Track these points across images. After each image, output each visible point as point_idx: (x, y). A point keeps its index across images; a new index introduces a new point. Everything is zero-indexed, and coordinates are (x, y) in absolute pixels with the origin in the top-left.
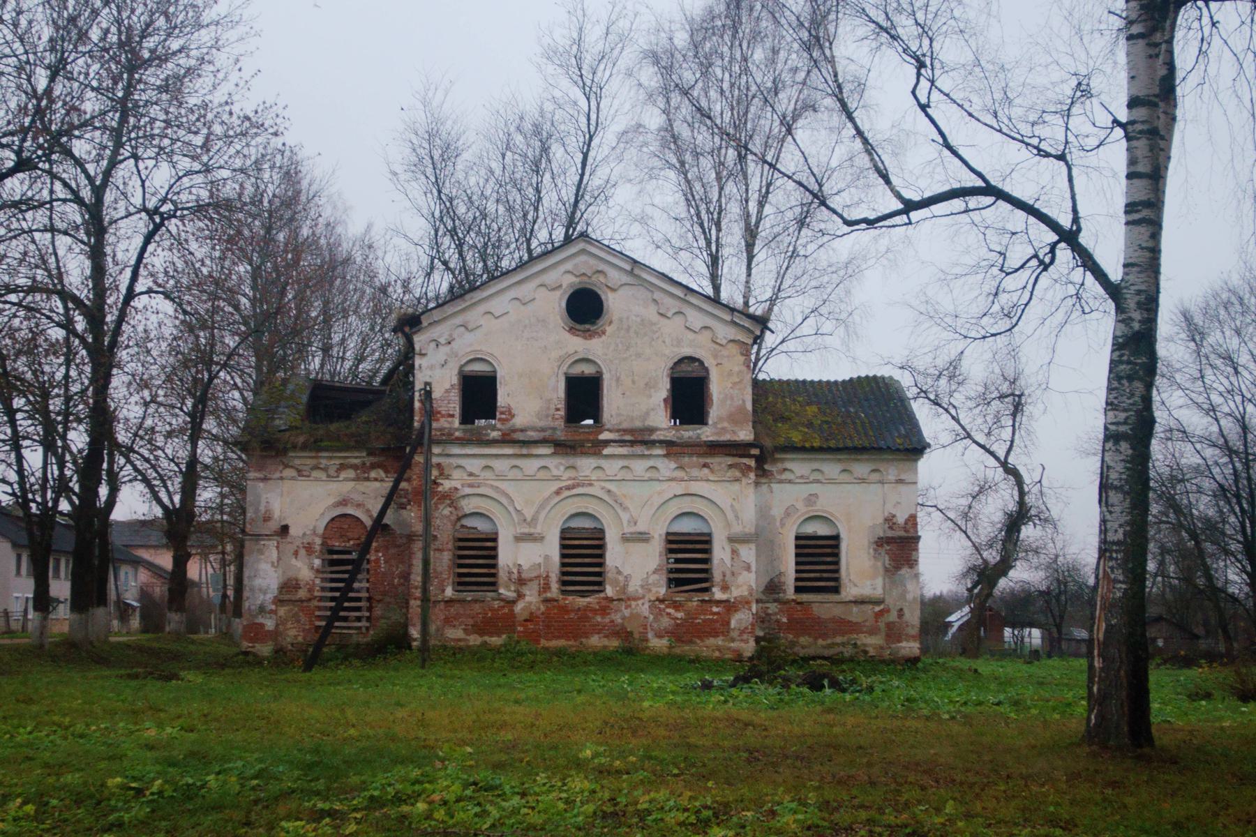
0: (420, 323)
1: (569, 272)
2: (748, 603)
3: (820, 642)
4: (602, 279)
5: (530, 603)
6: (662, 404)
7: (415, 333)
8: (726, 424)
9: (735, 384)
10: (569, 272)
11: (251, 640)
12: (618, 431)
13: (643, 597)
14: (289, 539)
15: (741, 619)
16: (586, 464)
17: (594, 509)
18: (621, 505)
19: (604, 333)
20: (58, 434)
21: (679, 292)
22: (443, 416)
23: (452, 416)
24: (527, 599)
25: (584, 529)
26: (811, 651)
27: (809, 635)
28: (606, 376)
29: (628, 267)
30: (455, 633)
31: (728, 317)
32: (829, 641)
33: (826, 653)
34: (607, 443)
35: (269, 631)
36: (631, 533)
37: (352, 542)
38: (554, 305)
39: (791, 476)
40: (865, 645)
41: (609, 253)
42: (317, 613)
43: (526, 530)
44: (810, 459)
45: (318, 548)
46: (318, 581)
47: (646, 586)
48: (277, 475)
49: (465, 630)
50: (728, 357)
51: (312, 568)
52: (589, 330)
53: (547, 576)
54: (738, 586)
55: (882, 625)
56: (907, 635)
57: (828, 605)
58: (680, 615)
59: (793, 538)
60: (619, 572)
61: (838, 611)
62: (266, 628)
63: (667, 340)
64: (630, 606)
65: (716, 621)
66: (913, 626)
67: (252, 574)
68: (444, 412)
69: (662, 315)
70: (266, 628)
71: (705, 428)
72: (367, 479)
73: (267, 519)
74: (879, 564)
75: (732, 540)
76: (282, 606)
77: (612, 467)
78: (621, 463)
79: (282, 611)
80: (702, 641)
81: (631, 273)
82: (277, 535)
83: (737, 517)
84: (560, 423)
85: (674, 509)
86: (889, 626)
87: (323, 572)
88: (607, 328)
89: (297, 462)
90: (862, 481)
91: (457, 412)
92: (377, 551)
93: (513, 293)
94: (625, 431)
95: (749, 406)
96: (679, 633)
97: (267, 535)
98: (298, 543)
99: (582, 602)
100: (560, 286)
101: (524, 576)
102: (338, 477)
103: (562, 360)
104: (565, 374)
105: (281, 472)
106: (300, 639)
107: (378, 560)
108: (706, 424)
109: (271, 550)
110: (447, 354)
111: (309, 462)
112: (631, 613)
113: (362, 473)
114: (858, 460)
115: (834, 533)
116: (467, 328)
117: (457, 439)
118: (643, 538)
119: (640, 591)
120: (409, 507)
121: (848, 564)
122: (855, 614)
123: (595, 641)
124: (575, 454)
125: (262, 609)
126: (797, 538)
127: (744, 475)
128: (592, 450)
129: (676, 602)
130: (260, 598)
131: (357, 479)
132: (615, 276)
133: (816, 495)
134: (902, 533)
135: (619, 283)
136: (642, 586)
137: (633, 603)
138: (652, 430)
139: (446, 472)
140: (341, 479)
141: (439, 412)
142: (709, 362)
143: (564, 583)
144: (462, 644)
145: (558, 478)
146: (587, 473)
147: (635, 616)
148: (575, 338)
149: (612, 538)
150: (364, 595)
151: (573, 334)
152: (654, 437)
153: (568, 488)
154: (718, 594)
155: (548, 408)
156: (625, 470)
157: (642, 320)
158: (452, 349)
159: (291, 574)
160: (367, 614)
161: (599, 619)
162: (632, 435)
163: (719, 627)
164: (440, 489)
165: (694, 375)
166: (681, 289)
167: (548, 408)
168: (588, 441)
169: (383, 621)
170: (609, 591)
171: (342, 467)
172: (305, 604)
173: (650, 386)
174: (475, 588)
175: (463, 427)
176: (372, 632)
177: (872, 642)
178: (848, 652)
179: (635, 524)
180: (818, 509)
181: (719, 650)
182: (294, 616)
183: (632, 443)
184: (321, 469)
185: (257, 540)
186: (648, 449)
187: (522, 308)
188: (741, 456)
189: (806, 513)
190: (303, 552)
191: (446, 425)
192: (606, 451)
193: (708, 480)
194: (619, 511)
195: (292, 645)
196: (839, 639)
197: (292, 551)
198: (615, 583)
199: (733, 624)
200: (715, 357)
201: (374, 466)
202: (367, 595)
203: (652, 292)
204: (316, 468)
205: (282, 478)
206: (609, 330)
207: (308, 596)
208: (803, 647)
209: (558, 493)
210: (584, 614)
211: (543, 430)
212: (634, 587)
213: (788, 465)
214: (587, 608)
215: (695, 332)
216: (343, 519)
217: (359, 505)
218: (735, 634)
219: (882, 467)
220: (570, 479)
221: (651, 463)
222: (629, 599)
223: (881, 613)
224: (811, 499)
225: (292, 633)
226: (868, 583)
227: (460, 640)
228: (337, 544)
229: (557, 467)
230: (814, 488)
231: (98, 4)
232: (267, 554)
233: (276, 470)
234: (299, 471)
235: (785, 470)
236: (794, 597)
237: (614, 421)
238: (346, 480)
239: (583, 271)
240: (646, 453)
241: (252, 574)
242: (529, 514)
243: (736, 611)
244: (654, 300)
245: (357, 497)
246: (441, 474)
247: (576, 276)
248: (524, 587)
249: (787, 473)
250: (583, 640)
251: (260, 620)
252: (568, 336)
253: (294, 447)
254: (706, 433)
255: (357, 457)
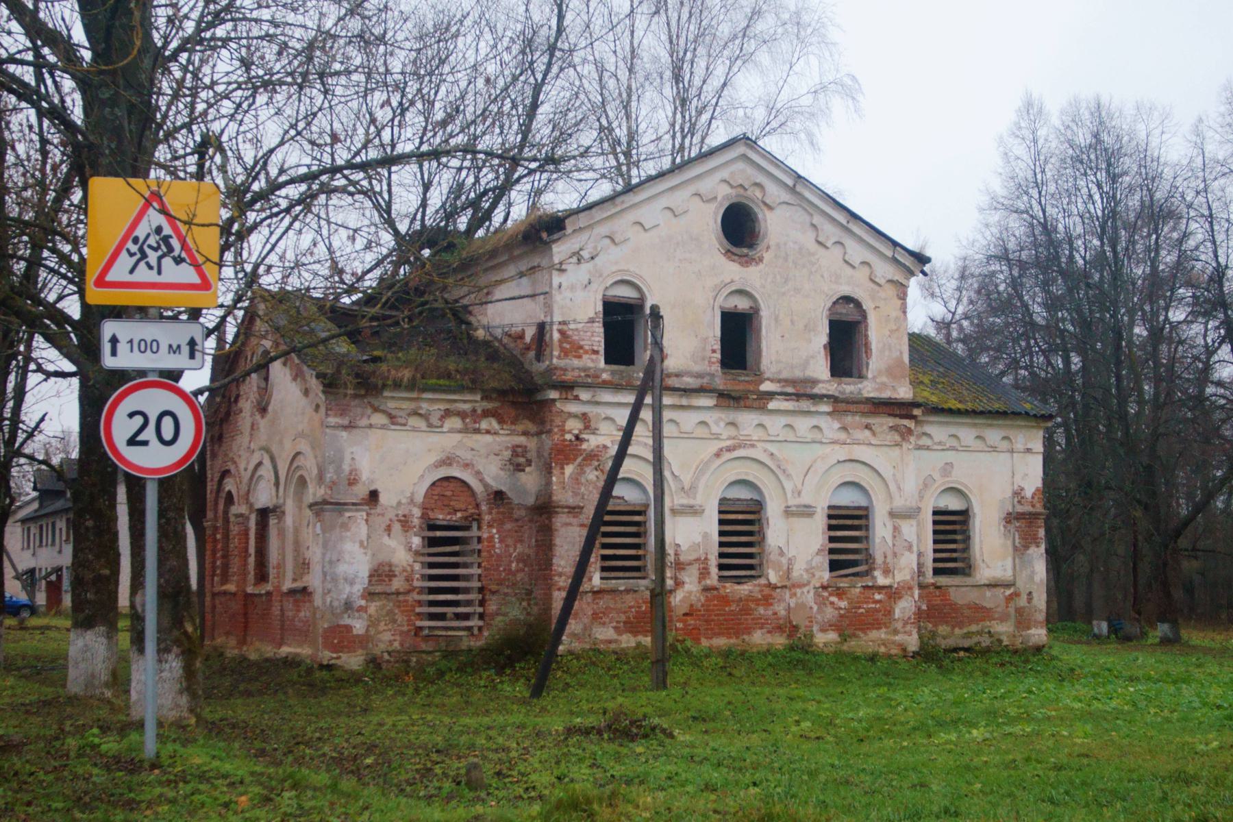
0: (563, 228)
1: (725, 181)
2: (910, 588)
3: (957, 631)
4: (758, 194)
5: (690, 593)
7: (555, 241)
8: (884, 379)
9: (891, 331)
10: (725, 181)
11: (336, 649)
12: (779, 381)
13: (808, 583)
14: (379, 510)
15: (905, 607)
16: (748, 420)
17: (756, 477)
18: (784, 471)
19: (761, 260)
20: (221, 341)
21: (841, 217)
22: (586, 352)
24: (687, 587)
25: (739, 500)
26: (951, 642)
27: (947, 623)
28: (765, 313)
29: (790, 182)
30: (604, 633)
31: (889, 253)
32: (965, 630)
33: (967, 643)
34: (771, 395)
35: (358, 636)
36: (798, 506)
37: (459, 515)
38: (709, 221)
40: (1000, 634)
41: (772, 162)
42: (418, 610)
43: (685, 501)
44: (947, 423)
46: (417, 567)
47: (810, 570)
48: (364, 422)
49: (616, 628)
50: (885, 299)
51: (410, 549)
52: (746, 256)
53: (706, 559)
54: (901, 570)
55: (1012, 610)
56: (1035, 621)
57: (964, 589)
58: (843, 604)
59: (931, 512)
60: (782, 553)
61: (972, 596)
62: (355, 632)
63: (826, 275)
64: (795, 594)
65: (878, 611)
66: (1041, 611)
67: (334, 558)
68: (587, 348)
70: (355, 632)
71: (865, 383)
72: (478, 431)
73: (353, 482)
74: (1009, 543)
75: (892, 515)
76: (373, 601)
77: (775, 424)
78: (784, 420)
79: (373, 608)
80: (866, 634)
81: (792, 190)
82: (366, 504)
85: (839, 476)
86: (1019, 611)
87: (423, 555)
89: (391, 405)
90: (994, 449)
91: (602, 349)
92: (490, 526)
93: (664, 201)
94: (787, 382)
95: (906, 358)
96: (850, 624)
97: (354, 504)
98: (391, 514)
99: (745, 589)
100: (716, 198)
101: (682, 558)
102: (442, 426)
103: (718, 290)
104: (721, 307)
105: (369, 417)
106: (396, 645)
107: (491, 538)
108: (861, 377)
109: (359, 525)
110: (590, 272)
111: (406, 405)
112: (797, 604)
113: (471, 427)
114: (990, 425)
115: (963, 508)
116: (613, 240)
117: (604, 382)
118: (806, 512)
119: (805, 576)
120: (528, 469)
121: (981, 541)
122: (991, 599)
123: (759, 638)
124: (737, 408)
125: (348, 606)
126: (935, 513)
127: (904, 439)
128: (756, 404)
129: (838, 588)
130: (346, 591)
131: (465, 430)
132: (774, 192)
133: (951, 465)
134: (1030, 509)
135: (778, 201)
136: (807, 570)
137: (798, 591)
138: (815, 382)
139: (593, 425)
140: (445, 429)
142: (867, 305)
143: (721, 567)
144: (613, 646)
147: (801, 606)
148: (732, 263)
149: (773, 510)
150: (476, 584)
151: (729, 258)
152: (816, 391)
153: (729, 449)
154: (882, 580)
156: (788, 429)
157: (801, 249)
158: (596, 265)
159: (382, 557)
160: (480, 610)
161: (761, 610)
162: (794, 387)
163: (879, 618)
164: (584, 446)
165: (850, 319)
166: (845, 214)
167: (704, 349)
168: (753, 392)
169: (500, 618)
170: (773, 577)
171: (448, 413)
172: (401, 598)
173: (809, 328)
174: (621, 574)
175: (608, 367)
176: (486, 634)
177: (1003, 629)
178: (986, 641)
179: (799, 493)
180: (952, 481)
181: (884, 644)
182: (390, 612)
183: (798, 396)
184: (420, 415)
185: (341, 513)
186: (814, 404)
187: (674, 221)
188: (902, 417)
189: (944, 483)
190: (397, 527)
191: (590, 364)
192: (772, 405)
193: (871, 444)
194: (782, 478)
195: (389, 653)
196: (974, 628)
197: (384, 526)
198: (778, 567)
199: (897, 613)
200: (873, 298)
201: (486, 414)
202: (479, 584)
203: (811, 215)
204: (415, 413)
205: (371, 426)
206: (767, 256)
207: (408, 587)
208: (944, 638)
209: (718, 455)
210: (746, 604)
211: (699, 376)
212: (798, 572)
213: (928, 429)
214: (750, 598)
215: (854, 267)
216: (445, 484)
217: (467, 465)
218: (899, 625)
219: (1011, 433)
221: (814, 421)
222: (794, 586)
223: (1010, 598)
224: (948, 468)
225: (387, 637)
226: (1000, 564)
227: (610, 642)
228: (440, 517)
229: (717, 423)
230: (950, 456)
232: (353, 529)
233: (362, 415)
234: (391, 417)
235: (925, 434)
236: (932, 581)
237: (774, 369)
238: (451, 431)
239: (740, 182)
240: (813, 409)
241: (334, 558)
243: (900, 598)
244: (814, 226)
245: (466, 456)
246: (587, 427)
247: (732, 187)
248: (683, 573)
250: (746, 637)
251: (346, 621)
253: (397, 385)
254: (868, 389)
255: (469, 401)
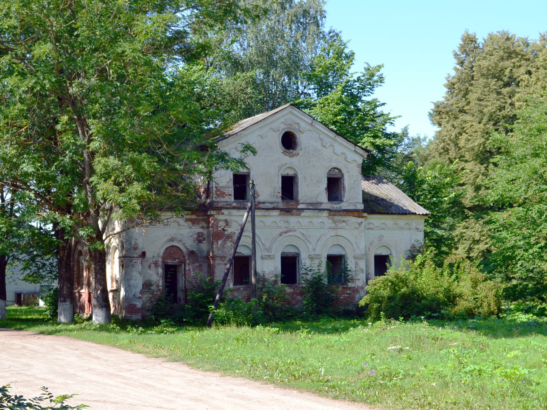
6: (324, 191)
14: (146, 259)
16: (293, 220)
19: (298, 154)
22: (226, 195)
23: (230, 195)
36: (314, 255)
37: (177, 260)
39: (373, 227)
45: (160, 263)
69: (323, 146)
71: (343, 203)
73: (135, 249)
83: (358, 247)
84: (280, 200)
88: (300, 152)
90: (402, 228)
98: (151, 261)
138: (321, 203)
141: (224, 193)
145: (280, 227)
146: (293, 225)
152: (322, 207)
155: (275, 192)
164: (226, 233)
165: (336, 176)
167: (275, 192)
175: (236, 201)
190: (153, 266)
191: (228, 200)
194: (308, 243)
197: (148, 265)
206: (301, 153)
213: (371, 221)
220: (285, 228)
224: (381, 238)
230: (382, 232)
231: (6, 59)
241: (129, 278)
242: (267, 245)
249: (370, 224)
252: (282, 155)
